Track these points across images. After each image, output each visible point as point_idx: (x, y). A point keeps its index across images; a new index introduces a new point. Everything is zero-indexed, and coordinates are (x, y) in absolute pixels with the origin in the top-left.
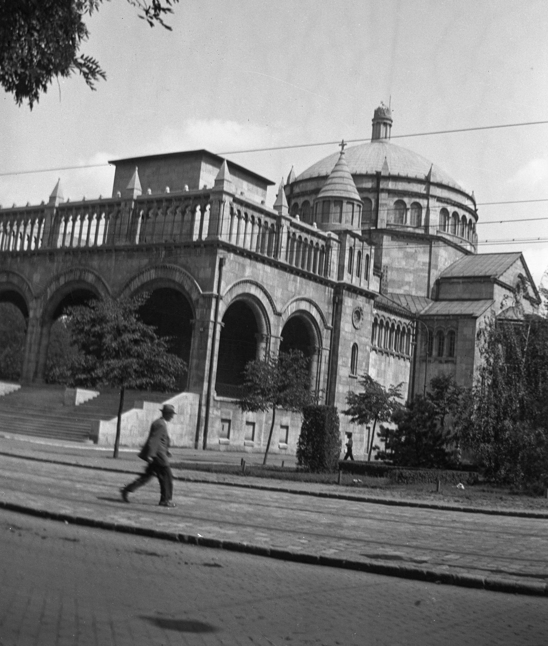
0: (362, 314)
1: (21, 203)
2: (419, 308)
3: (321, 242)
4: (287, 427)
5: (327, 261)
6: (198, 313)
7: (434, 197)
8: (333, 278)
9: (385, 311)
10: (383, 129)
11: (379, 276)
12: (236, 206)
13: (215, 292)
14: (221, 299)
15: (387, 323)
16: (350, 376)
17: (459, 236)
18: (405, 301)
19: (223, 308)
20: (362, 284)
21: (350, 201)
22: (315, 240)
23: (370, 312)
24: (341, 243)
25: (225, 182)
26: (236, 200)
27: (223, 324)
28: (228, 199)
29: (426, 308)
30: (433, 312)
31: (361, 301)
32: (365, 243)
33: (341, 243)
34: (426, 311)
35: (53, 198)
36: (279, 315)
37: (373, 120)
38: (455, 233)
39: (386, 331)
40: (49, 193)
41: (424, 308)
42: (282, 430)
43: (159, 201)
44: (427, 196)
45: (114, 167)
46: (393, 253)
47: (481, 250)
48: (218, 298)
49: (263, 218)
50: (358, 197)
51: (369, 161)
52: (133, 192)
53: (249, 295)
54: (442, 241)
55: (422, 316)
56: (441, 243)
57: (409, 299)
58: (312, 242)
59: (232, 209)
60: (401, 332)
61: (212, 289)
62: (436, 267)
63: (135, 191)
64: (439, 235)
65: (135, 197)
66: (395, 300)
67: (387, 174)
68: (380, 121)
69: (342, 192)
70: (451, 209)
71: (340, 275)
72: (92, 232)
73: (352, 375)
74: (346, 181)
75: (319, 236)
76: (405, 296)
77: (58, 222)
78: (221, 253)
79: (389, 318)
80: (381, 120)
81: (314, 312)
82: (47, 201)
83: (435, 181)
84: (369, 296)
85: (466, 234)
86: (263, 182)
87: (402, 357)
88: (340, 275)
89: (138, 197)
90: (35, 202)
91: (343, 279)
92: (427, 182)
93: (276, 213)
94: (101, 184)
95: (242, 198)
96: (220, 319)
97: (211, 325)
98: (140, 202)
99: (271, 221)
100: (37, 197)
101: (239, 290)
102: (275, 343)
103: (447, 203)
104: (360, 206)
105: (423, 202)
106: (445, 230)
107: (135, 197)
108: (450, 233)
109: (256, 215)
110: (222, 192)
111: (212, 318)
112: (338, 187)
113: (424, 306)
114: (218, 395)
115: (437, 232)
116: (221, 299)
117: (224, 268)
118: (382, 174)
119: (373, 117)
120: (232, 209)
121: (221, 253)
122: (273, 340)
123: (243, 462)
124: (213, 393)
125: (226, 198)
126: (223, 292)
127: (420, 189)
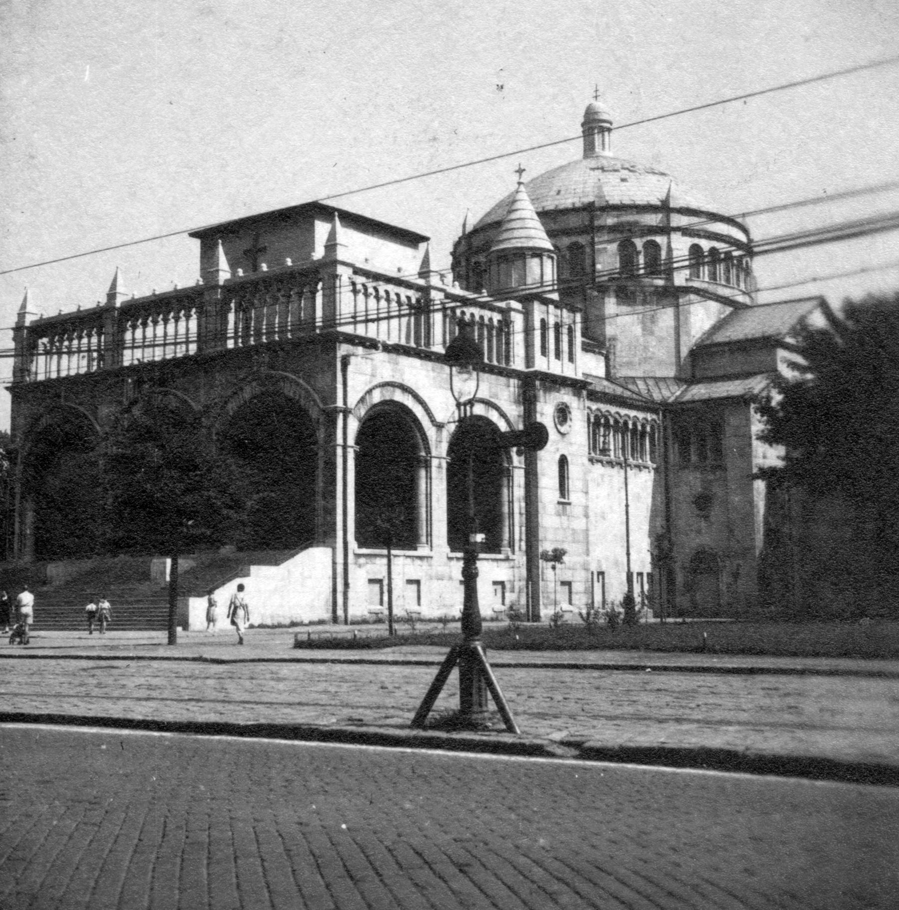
0: (570, 413)
1: (69, 308)
2: (666, 393)
3: (496, 317)
4: (418, 582)
5: (508, 343)
6: (321, 435)
7: (678, 229)
8: (518, 364)
9: (611, 404)
10: (597, 138)
11: (602, 354)
12: (360, 280)
13: (340, 403)
14: (350, 412)
15: (616, 422)
16: (559, 503)
17: (723, 283)
18: (644, 387)
19: (353, 426)
20: (565, 370)
21: (538, 253)
22: (487, 314)
23: (580, 410)
24: (527, 315)
25: (339, 247)
26: (357, 271)
27: (357, 448)
28: (344, 273)
29: (678, 393)
30: (688, 397)
31: (566, 397)
32: (564, 311)
33: (527, 315)
34: (677, 398)
35: (112, 296)
36: (440, 426)
37: (583, 125)
38: (715, 279)
39: (616, 432)
40: (106, 289)
41: (673, 394)
42: (409, 586)
43: (255, 284)
44: (666, 230)
45: (196, 244)
46: (621, 321)
47: (763, 298)
48: (346, 412)
49: (404, 292)
50: (547, 244)
51: (578, 188)
52: (217, 277)
53: (392, 402)
54: (692, 292)
55: (671, 405)
56: (692, 297)
57: (651, 383)
58: (482, 317)
59: (354, 284)
60: (638, 435)
61: (335, 402)
62: (688, 334)
63: (221, 273)
64: (690, 284)
65: (221, 283)
66: (630, 386)
67: (604, 204)
68: (594, 125)
69: (523, 240)
70: (706, 245)
71: (529, 359)
72: (176, 337)
73: (562, 500)
74: (530, 223)
75: (492, 309)
76: (644, 379)
77: (123, 331)
78: (343, 349)
79: (618, 413)
80: (593, 126)
81: (494, 416)
82: (103, 301)
83: (678, 206)
84: (578, 386)
85: (733, 279)
86: (411, 239)
87: (646, 467)
88: (529, 359)
89: (226, 281)
90: (88, 304)
91: (533, 366)
92: (664, 207)
93: (421, 282)
94: (182, 270)
95: (367, 267)
96: (351, 441)
97: (339, 451)
98: (231, 289)
99: (414, 295)
100: (91, 298)
101: (377, 397)
102: (440, 467)
103: (699, 236)
104: (552, 258)
105: (660, 240)
106: (698, 277)
107: (221, 283)
108: (707, 279)
109: (392, 288)
110: (335, 263)
111: (340, 441)
112: (516, 233)
113: (673, 391)
114: (361, 545)
115: (687, 280)
116: (350, 412)
117: (350, 368)
118: (597, 204)
119: (582, 120)
120: (354, 284)
121: (343, 349)
122: (435, 462)
123: (309, 634)
124: (353, 545)
125: (340, 270)
126: (352, 401)
127: (652, 219)
